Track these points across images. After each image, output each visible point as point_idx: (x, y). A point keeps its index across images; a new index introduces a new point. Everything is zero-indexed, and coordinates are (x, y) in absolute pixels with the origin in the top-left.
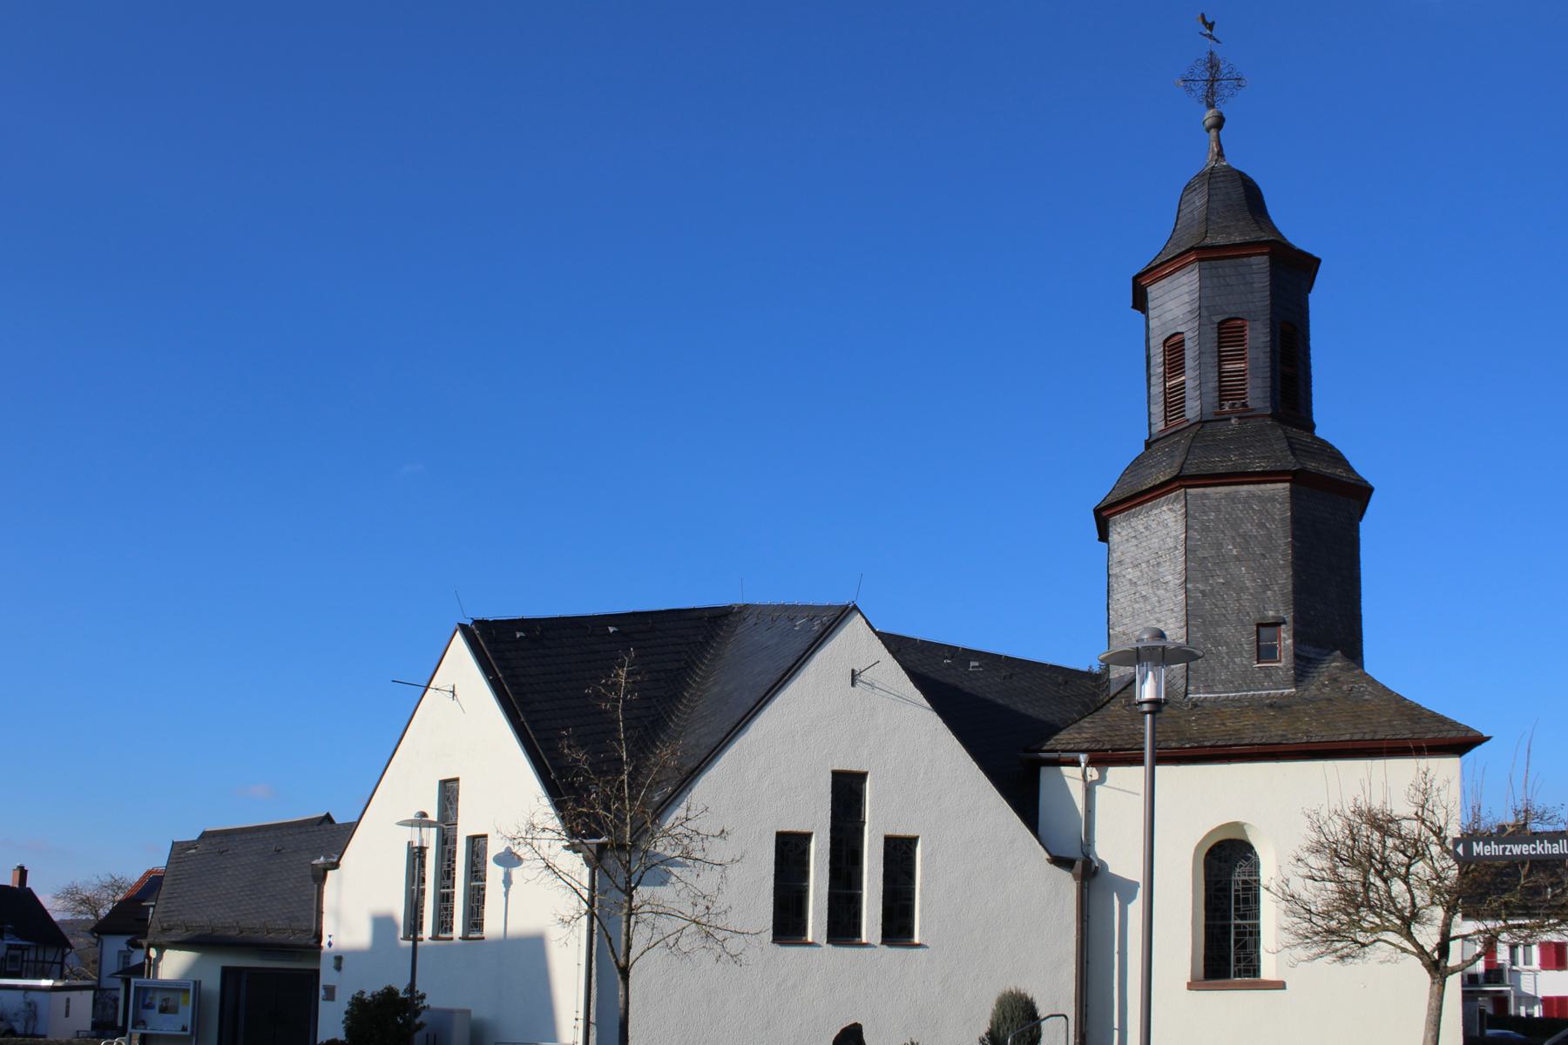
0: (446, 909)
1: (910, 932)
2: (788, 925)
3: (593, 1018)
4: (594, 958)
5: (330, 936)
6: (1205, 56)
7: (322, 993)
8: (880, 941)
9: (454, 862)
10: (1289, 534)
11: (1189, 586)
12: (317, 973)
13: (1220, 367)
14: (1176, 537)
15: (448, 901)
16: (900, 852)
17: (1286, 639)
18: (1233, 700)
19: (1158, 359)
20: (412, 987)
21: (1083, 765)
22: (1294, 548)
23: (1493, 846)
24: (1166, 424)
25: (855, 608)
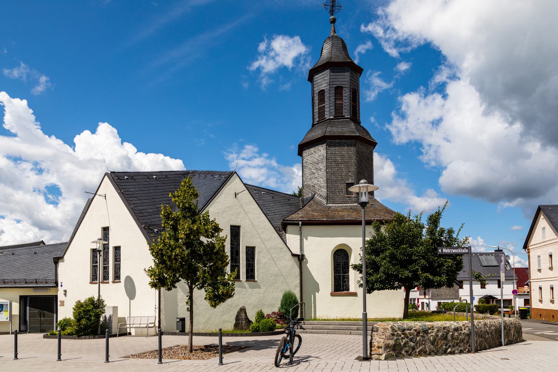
0: (106, 272)
1: (239, 278)
5: (61, 283)
7: (59, 303)
9: (108, 255)
11: (327, 170)
12: (56, 296)
13: (335, 101)
15: (106, 269)
16: (251, 251)
18: (340, 206)
19: (316, 98)
20: (99, 299)
21: (300, 225)
23: (461, 250)
25: (235, 172)
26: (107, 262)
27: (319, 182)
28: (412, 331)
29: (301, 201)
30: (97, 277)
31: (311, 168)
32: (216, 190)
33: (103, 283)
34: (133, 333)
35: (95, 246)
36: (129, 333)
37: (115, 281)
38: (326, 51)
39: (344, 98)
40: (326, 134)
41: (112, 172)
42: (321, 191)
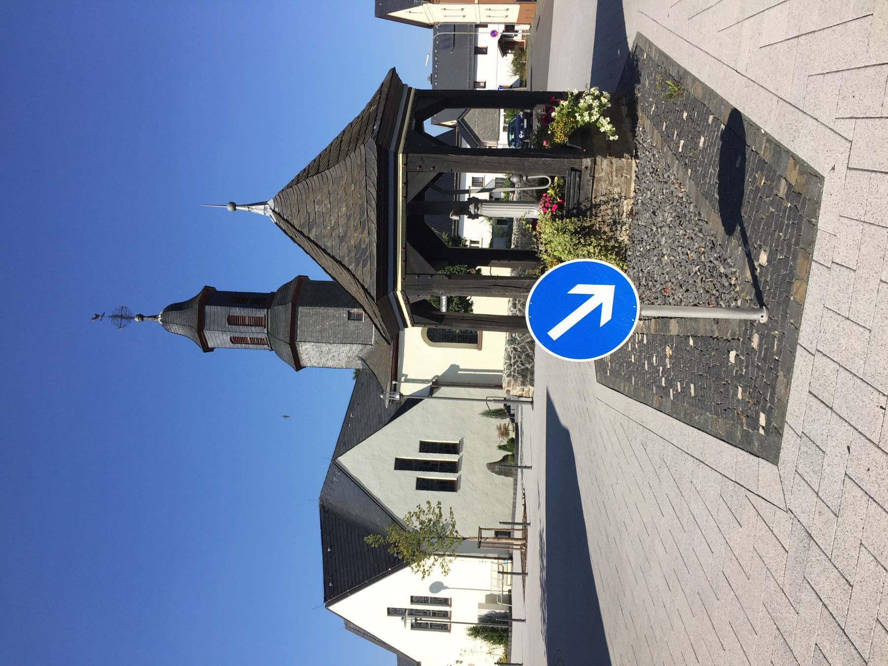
0: (439, 614)
1: (455, 463)
2: (450, 487)
3: (483, 555)
4: (462, 554)
6: (110, 319)
8: (457, 455)
9: (420, 610)
10: (315, 307)
13: (246, 325)
14: (313, 346)
16: (425, 447)
17: (355, 311)
21: (397, 383)
22: (321, 306)
24: (266, 344)
26: (428, 612)
27: (345, 352)
28: (512, 355)
30: (444, 625)
33: (450, 618)
34: (510, 588)
35: (409, 625)
36: (509, 593)
37: (449, 604)
38: (181, 331)
39: (242, 314)
40: (288, 342)
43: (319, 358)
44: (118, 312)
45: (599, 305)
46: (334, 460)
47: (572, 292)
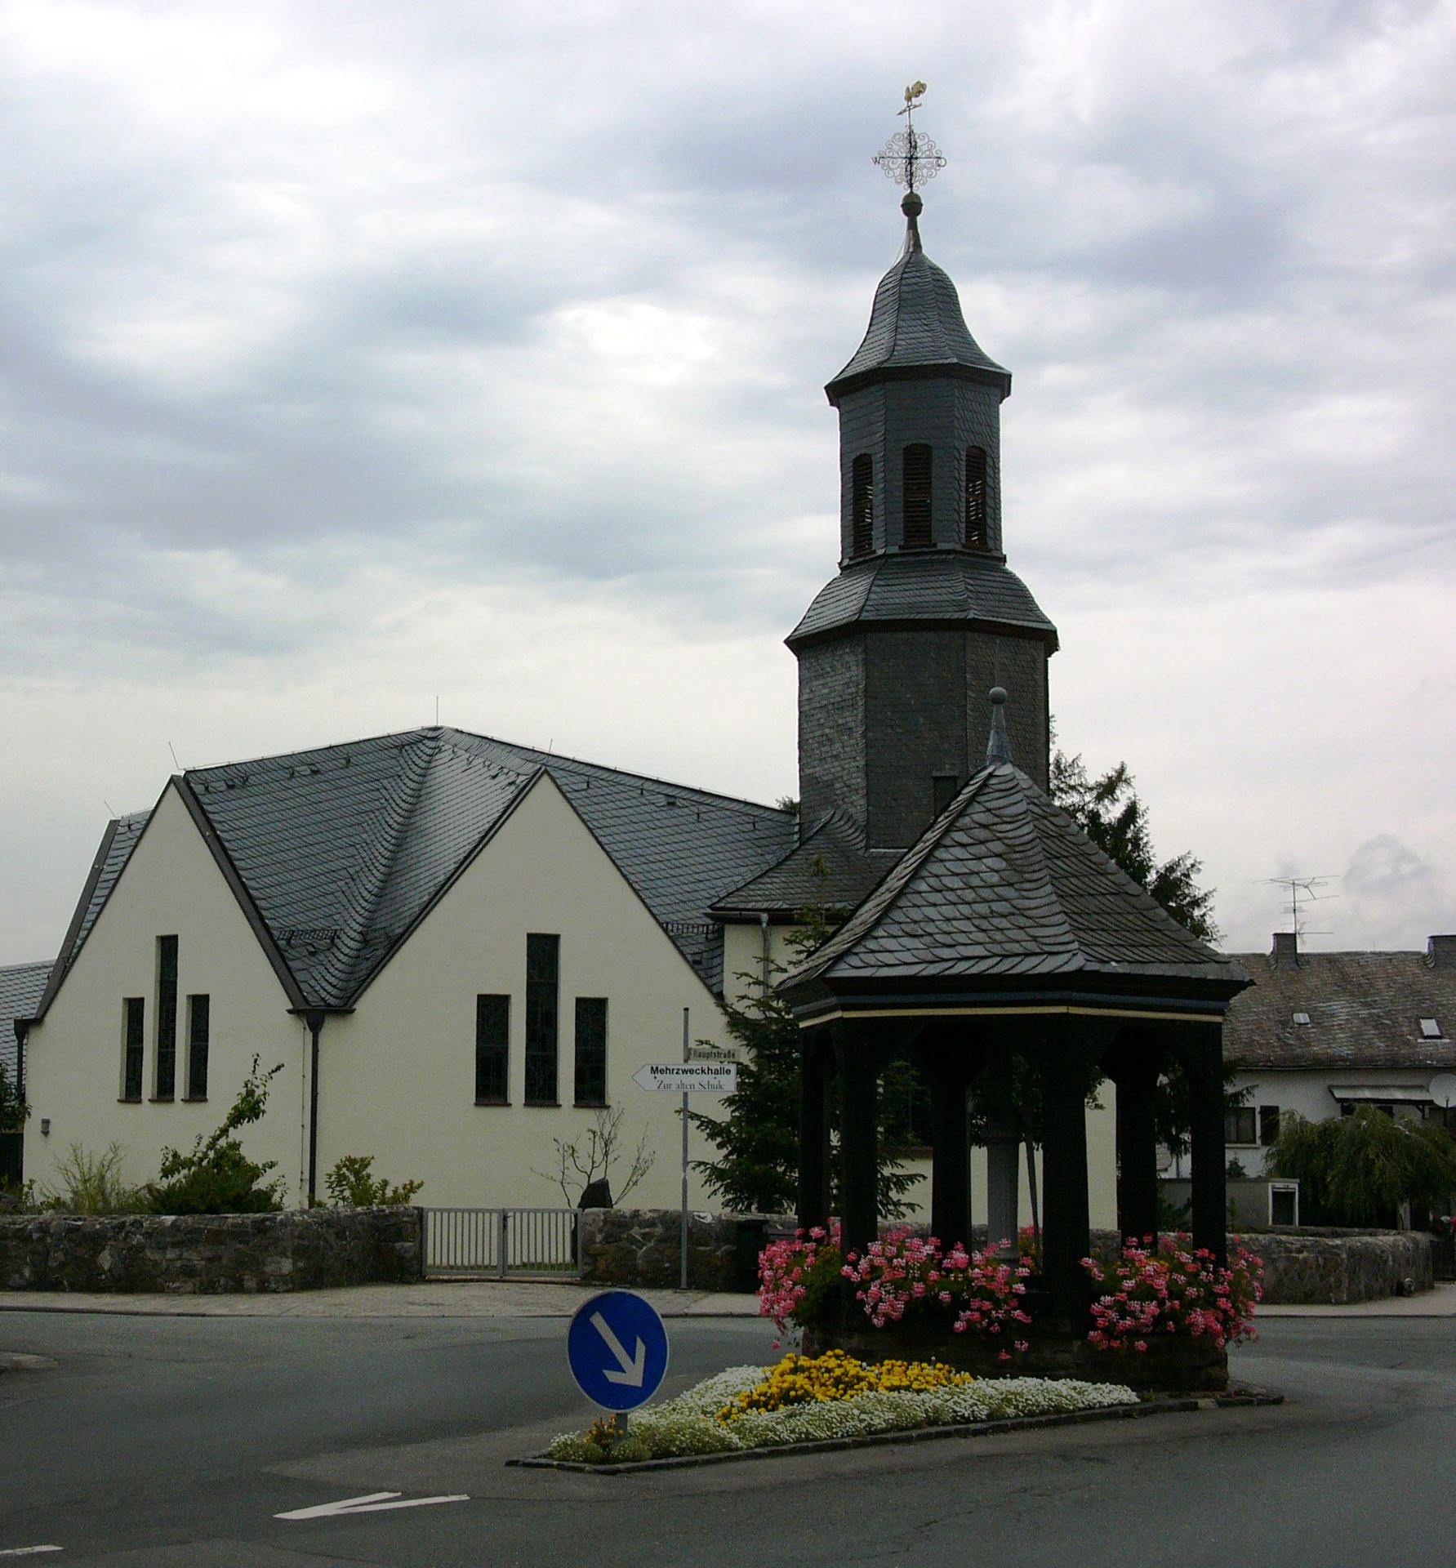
21: (764, 925)
29: (796, 829)
31: (822, 721)
32: (488, 826)
41: (188, 772)
42: (852, 803)
43: (824, 703)
44: (925, 148)
45: (620, 1365)
46: (546, 772)
47: (639, 1341)
